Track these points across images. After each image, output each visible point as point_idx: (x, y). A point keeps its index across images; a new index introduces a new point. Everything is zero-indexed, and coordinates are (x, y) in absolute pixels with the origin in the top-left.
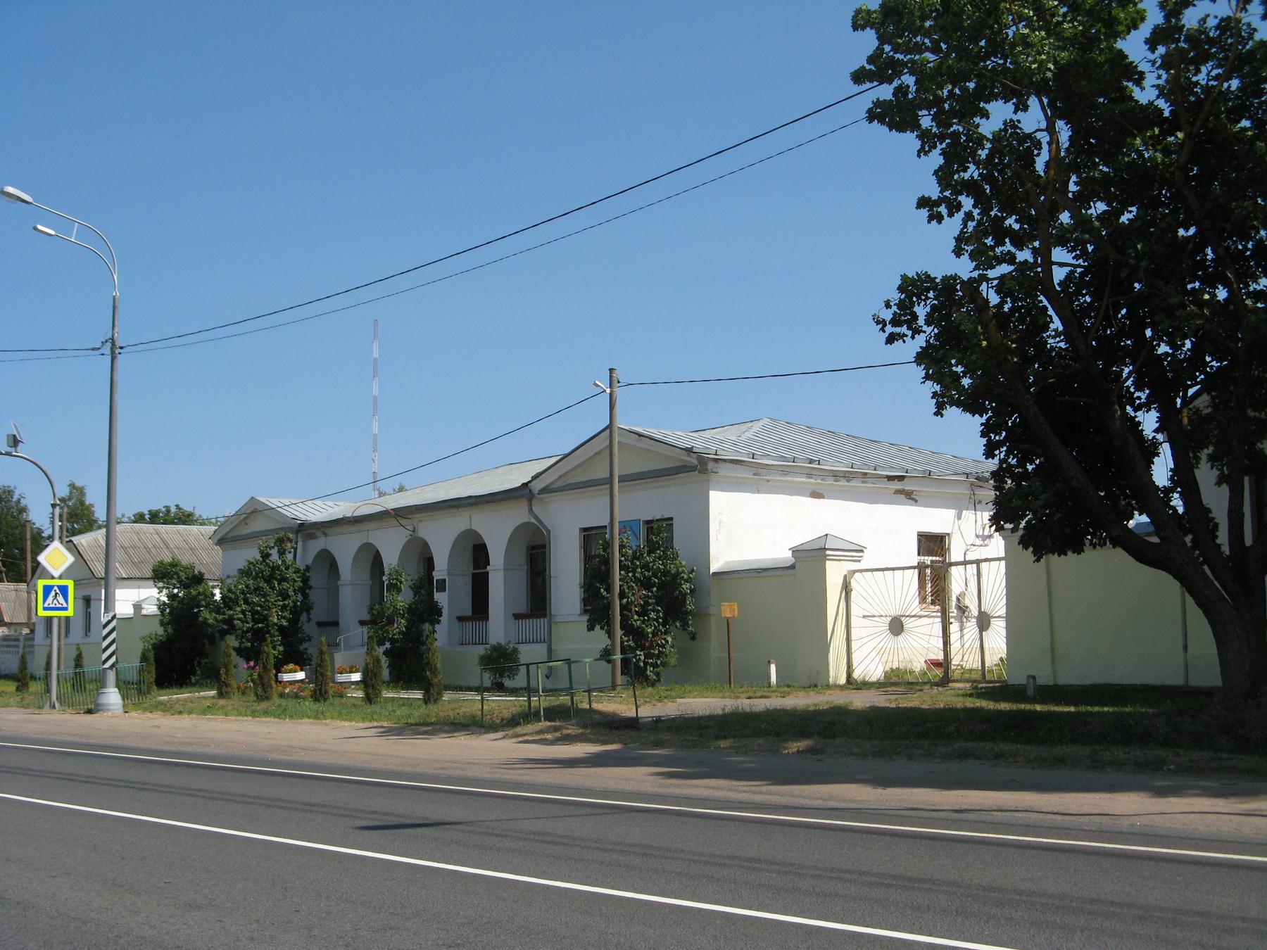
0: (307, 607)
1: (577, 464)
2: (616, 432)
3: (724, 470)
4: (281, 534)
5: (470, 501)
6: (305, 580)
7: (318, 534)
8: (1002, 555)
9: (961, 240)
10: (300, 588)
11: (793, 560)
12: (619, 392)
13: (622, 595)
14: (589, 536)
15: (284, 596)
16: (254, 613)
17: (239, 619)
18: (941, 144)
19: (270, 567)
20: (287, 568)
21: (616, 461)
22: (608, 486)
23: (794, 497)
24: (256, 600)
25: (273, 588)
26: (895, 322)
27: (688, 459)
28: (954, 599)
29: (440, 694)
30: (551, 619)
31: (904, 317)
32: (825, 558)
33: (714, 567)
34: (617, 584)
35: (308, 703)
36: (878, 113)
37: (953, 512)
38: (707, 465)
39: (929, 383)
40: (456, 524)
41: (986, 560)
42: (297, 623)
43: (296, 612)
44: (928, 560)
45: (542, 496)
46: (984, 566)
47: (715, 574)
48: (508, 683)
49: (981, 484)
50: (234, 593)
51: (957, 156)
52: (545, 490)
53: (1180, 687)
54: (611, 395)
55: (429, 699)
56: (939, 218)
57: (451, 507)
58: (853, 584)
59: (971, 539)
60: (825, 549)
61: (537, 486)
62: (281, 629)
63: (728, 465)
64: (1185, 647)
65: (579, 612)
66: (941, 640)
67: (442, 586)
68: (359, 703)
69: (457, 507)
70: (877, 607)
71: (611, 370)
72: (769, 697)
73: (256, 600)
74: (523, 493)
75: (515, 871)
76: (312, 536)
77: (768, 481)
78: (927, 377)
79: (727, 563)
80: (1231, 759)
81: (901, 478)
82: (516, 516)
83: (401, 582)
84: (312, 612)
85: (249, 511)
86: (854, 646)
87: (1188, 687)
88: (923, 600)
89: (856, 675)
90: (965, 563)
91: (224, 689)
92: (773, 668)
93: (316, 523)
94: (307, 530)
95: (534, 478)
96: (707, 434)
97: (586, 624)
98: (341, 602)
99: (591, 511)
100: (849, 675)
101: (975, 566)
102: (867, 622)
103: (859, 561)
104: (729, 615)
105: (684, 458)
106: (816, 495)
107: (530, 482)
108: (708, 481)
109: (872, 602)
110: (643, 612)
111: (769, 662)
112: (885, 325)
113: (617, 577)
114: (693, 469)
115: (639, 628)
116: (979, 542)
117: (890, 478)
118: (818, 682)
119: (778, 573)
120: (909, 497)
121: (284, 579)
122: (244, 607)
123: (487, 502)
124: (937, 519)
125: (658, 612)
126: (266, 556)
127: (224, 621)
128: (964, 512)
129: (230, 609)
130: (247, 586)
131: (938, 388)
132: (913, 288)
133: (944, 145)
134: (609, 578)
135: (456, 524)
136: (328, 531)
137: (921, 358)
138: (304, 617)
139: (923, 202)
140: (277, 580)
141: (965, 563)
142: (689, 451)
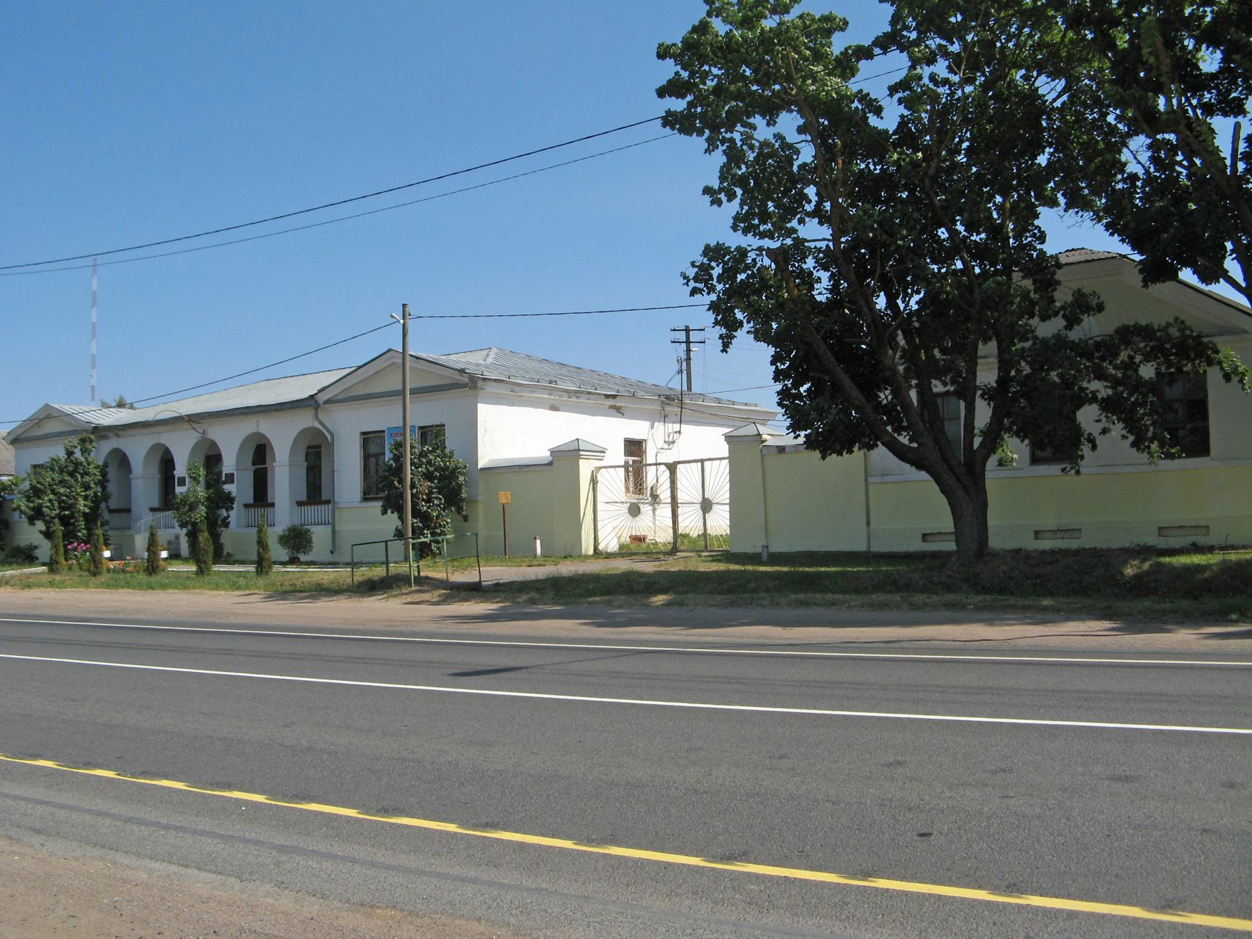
0: (106, 497)
1: (359, 380)
2: (408, 358)
3: (490, 388)
4: (85, 435)
5: (259, 409)
6: (104, 474)
7: (111, 435)
8: (727, 455)
9: (737, 219)
10: (99, 480)
11: (551, 458)
12: (410, 323)
13: (413, 486)
14: (368, 438)
15: (86, 487)
16: (60, 502)
17: (47, 507)
18: (722, 145)
19: (73, 463)
20: (89, 464)
21: (408, 378)
22: (401, 397)
23: (538, 410)
24: (62, 490)
25: (76, 481)
26: (696, 279)
27: (460, 378)
28: (649, 489)
29: (270, 567)
30: (334, 506)
31: (703, 275)
32: (579, 457)
33: (481, 464)
34: (409, 476)
35: (143, 577)
36: (669, 120)
37: (648, 423)
38: (477, 383)
39: (718, 327)
40: (247, 427)
41: (709, 459)
42: (98, 510)
43: (96, 502)
44: (631, 459)
45: (327, 406)
46: (707, 464)
47: (482, 469)
48: (303, 558)
49: (669, 402)
50: (42, 484)
51: (734, 156)
52: (328, 402)
53: (864, 552)
54: (404, 325)
55: (262, 571)
56: (719, 203)
57: (242, 414)
58: (599, 477)
59: (661, 444)
60: (579, 450)
61: (322, 398)
62: (85, 514)
63: (493, 383)
64: (868, 523)
65: (359, 500)
66: (671, 520)
67: (230, 479)
68: (193, 576)
69: (246, 414)
70: (619, 496)
71: (404, 305)
72: (545, 565)
73: (62, 490)
74: (310, 403)
75: (1068, 717)
76: (105, 437)
77: (520, 396)
78: (716, 323)
79: (491, 461)
80: (1008, 599)
81: (614, 397)
82: (304, 421)
83: (200, 476)
84: (109, 500)
85: (42, 417)
86: (600, 526)
87: (870, 552)
88: (627, 489)
89: (601, 547)
90: (657, 464)
91: (55, 566)
92: (538, 542)
93: (109, 427)
94: (101, 432)
95: (320, 391)
96: (452, 357)
97: (380, 509)
98: (133, 495)
99: (382, 418)
100: (596, 548)
101: (699, 464)
102: (611, 507)
103: (602, 460)
104: (504, 501)
105: (457, 377)
106: (554, 408)
107: (316, 394)
108: (477, 396)
109: (614, 491)
110: (429, 500)
111: (535, 538)
112: (689, 281)
113: (409, 472)
114: (464, 386)
115: (426, 512)
116: (666, 446)
117: (607, 396)
118: (572, 553)
119: (537, 469)
120: (619, 411)
121: (87, 474)
122: (52, 497)
123: (276, 410)
124: (637, 429)
125: (440, 499)
126: (70, 453)
127: (32, 509)
128: (656, 424)
129: (39, 498)
130: (53, 479)
131: (724, 331)
132: (714, 252)
133: (725, 147)
134: (402, 472)
135: (247, 427)
136: (121, 433)
137: (713, 307)
138: (103, 505)
139: (707, 191)
140: (80, 473)
141: (657, 464)
142: (462, 371)
